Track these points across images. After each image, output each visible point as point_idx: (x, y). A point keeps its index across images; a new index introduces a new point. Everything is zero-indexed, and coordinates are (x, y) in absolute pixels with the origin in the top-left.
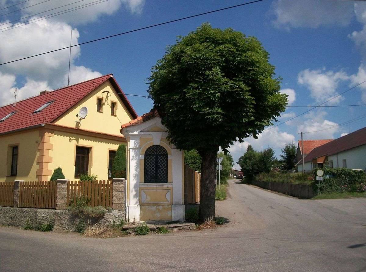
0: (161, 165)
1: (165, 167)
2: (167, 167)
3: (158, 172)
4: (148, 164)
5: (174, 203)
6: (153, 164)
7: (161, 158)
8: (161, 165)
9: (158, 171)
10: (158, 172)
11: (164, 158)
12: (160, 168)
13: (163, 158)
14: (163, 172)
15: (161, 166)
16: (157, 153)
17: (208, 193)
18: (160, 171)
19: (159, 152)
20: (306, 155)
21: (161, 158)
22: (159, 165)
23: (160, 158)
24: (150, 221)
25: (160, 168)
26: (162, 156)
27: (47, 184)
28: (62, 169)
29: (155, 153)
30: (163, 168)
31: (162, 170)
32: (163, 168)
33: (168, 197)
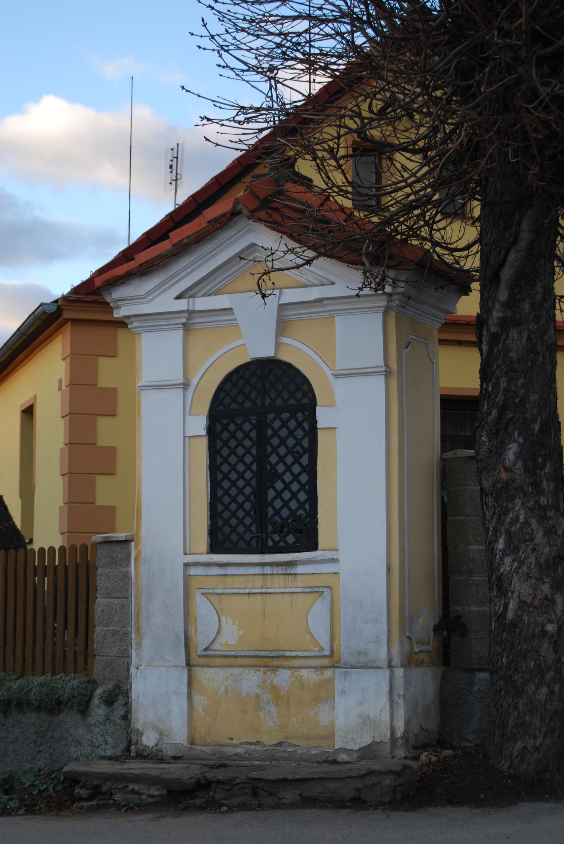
0: (281, 459)
1: (304, 469)
2: (311, 470)
3: (295, 402)
4: (226, 476)
5: (345, 655)
6: (247, 443)
7: (284, 424)
8: (281, 459)
9: (271, 494)
10: (295, 402)
11: (300, 425)
12: (279, 477)
13: (292, 424)
14: (294, 495)
15: (281, 468)
16: (268, 401)
17: (506, 606)
18: (279, 494)
19: (273, 394)
20: (96, 624)
21: (284, 424)
22: (274, 459)
23: (277, 424)
24: (235, 746)
25: (279, 477)
26: (285, 416)
27: (46, 578)
28: (52, 545)
29: (259, 402)
30: (296, 478)
31: (287, 486)
32: (296, 478)
33: (319, 626)
